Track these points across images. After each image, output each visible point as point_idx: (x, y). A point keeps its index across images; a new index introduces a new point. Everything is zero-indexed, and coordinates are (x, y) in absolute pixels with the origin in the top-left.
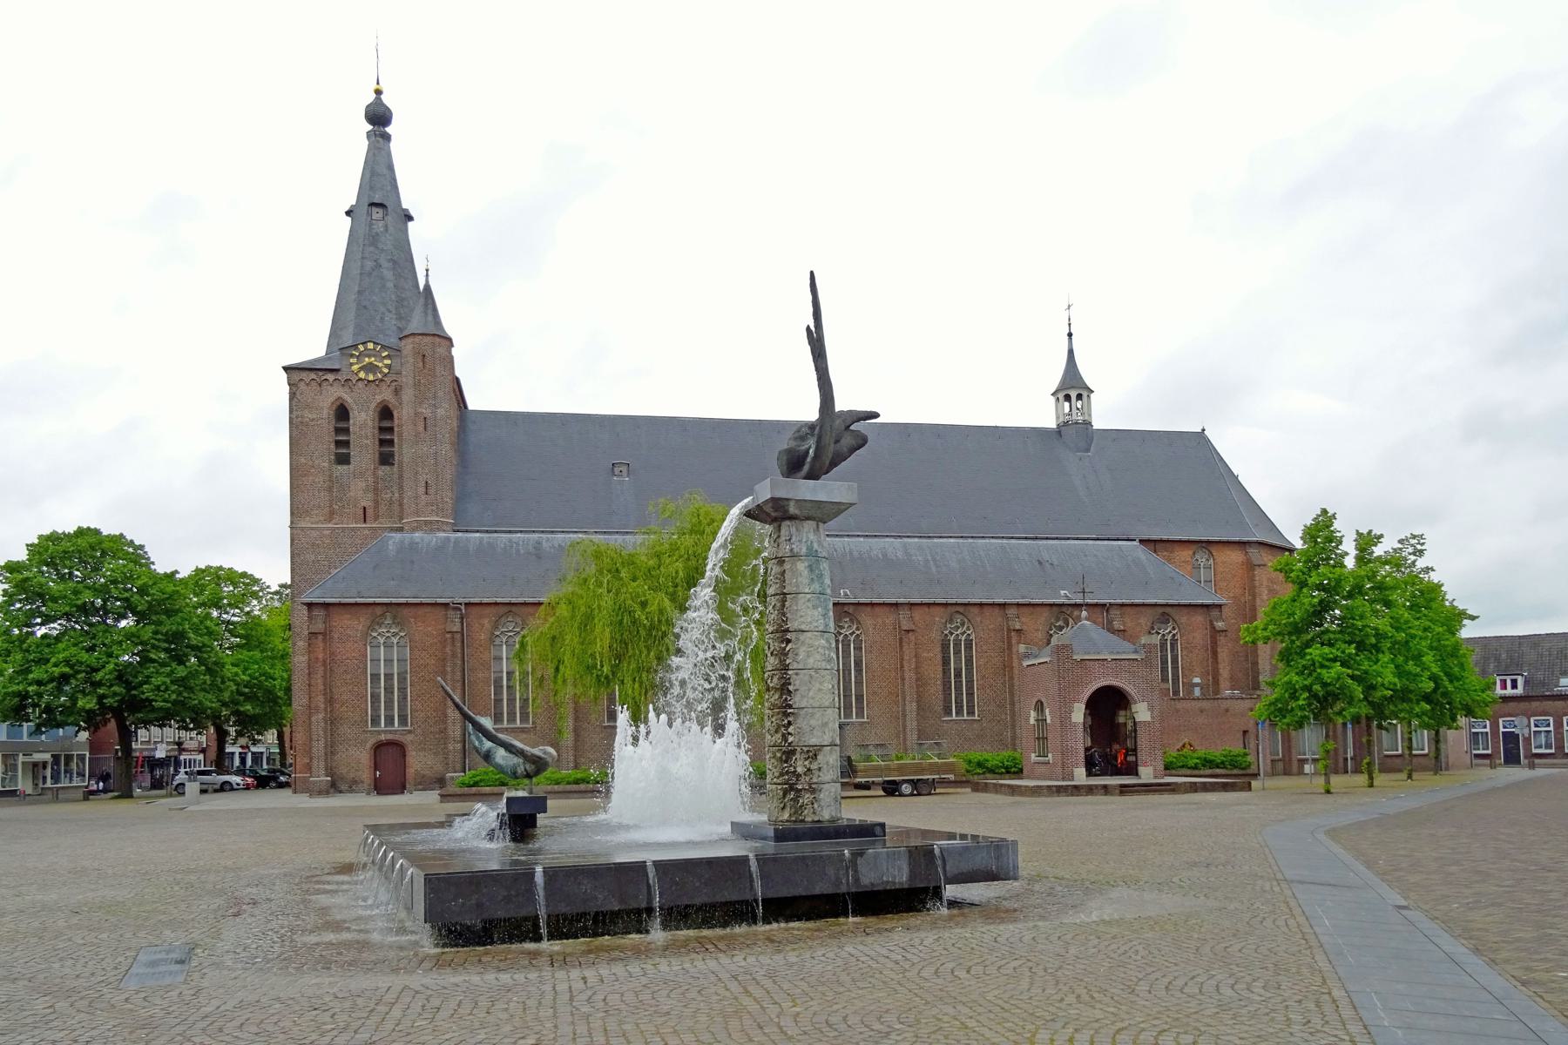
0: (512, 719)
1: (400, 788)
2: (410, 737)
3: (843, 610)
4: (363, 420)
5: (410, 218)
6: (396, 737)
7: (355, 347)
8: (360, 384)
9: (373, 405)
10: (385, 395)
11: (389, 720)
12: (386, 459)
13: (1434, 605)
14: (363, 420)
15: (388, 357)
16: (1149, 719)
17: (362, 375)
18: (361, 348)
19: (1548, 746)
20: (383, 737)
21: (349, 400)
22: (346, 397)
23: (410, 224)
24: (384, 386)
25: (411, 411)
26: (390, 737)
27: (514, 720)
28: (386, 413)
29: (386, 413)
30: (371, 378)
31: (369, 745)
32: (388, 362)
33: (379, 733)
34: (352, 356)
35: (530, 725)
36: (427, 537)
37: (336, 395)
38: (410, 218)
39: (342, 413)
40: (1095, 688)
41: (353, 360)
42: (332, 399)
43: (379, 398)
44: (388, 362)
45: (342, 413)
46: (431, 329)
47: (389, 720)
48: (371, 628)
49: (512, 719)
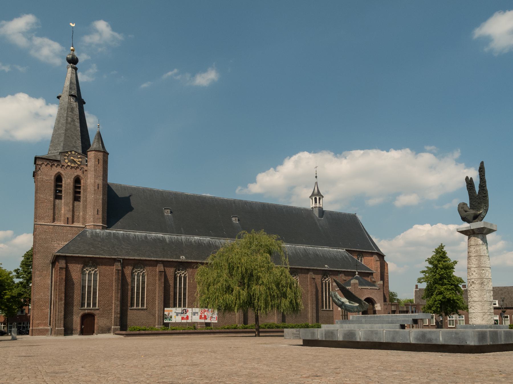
0: (138, 305)
1: (71, 334)
2: (98, 312)
3: (160, 272)
4: (67, 182)
5: (85, 103)
6: (92, 311)
10: (79, 172)
11: (89, 305)
12: (76, 198)
14: (67, 182)
15: (80, 158)
16: (380, 309)
17: (69, 164)
18: (69, 153)
20: (86, 311)
21: (63, 173)
22: (61, 172)
23: (84, 105)
24: (78, 170)
25: (92, 181)
26: (89, 311)
27: (139, 306)
28: (77, 180)
29: (77, 180)
30: (73, 165)
31: (80, 315)
32: (80, 160)
33: (85, 309)
34: (65, 156)
35: (145, 308)
36: (102, 231)
37: (57, 171)
39: (58, 179)
40: (368, 297)
41: (66, 158)
42: (56, 172)
43: (76, 174)
44: (80, 160)
45: (58, 179)
46: (102, 149)
47: (89, 305)
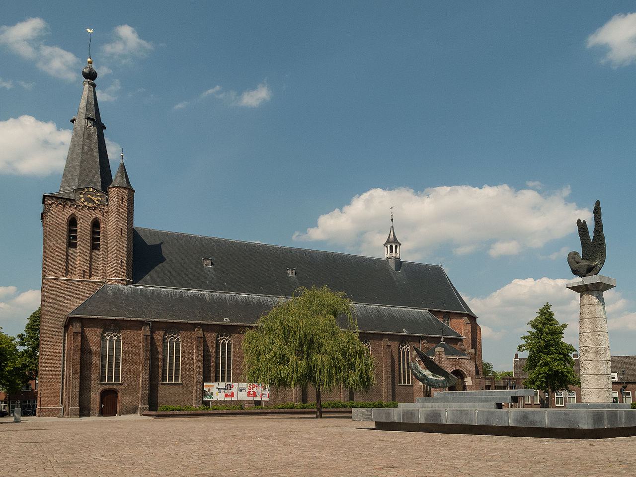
2: (121, 387)
4: (84, 227)
5: (105, 128)
7: (83, 189)
8: (84, 209)
9: (91, 220)
11: (110, 379)
12: (95, 246)
13: (281, 387)
14: (84, 227)
15: (100, 196)
17: (86, 203)
18: (91, 190)
19: (562, 404)
20: (107, 387)
22: (76, 213)
27: (172, 380)
28: (96, 224)
29: (96, 224)
30: (90, 205)
34: (81, 193)
36: (127, 287)
37: (71, 212)
38: (105, 128)
39: (73, 222)
43: (94, 216)
45: (73, 222)
46: (126, 185)
47: (110, 379)
48: (104, 332)
49: (170, 379)
